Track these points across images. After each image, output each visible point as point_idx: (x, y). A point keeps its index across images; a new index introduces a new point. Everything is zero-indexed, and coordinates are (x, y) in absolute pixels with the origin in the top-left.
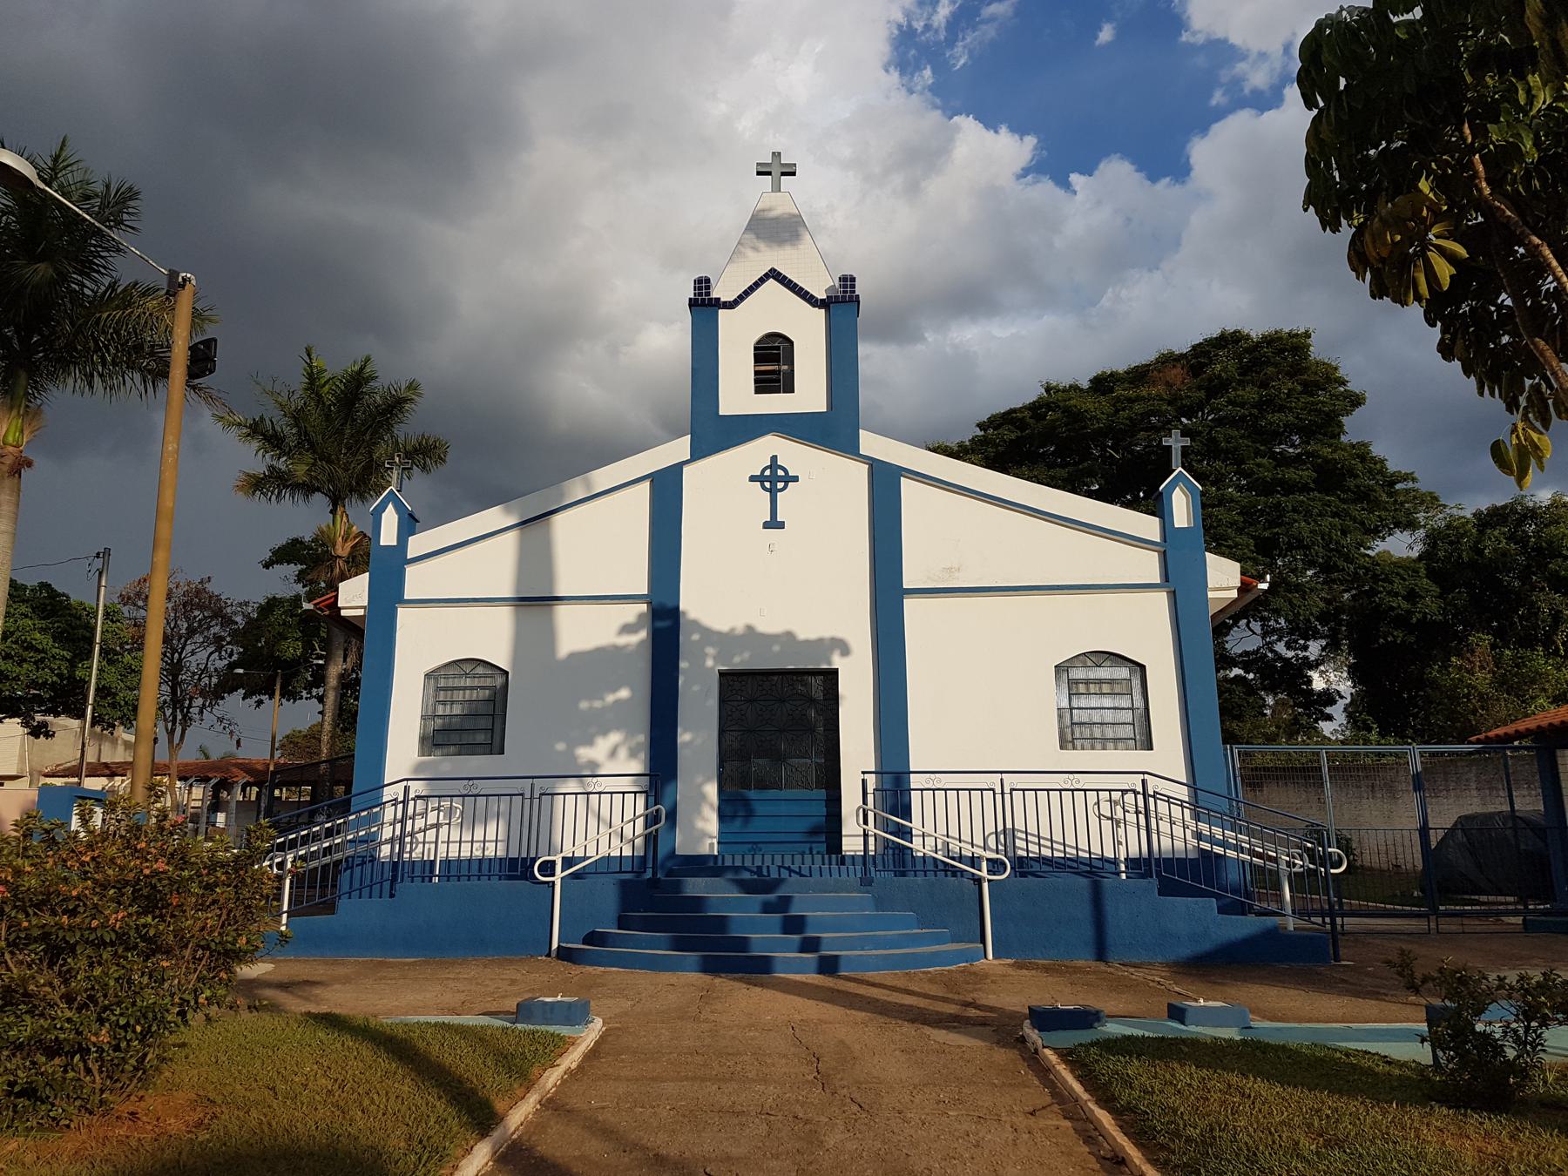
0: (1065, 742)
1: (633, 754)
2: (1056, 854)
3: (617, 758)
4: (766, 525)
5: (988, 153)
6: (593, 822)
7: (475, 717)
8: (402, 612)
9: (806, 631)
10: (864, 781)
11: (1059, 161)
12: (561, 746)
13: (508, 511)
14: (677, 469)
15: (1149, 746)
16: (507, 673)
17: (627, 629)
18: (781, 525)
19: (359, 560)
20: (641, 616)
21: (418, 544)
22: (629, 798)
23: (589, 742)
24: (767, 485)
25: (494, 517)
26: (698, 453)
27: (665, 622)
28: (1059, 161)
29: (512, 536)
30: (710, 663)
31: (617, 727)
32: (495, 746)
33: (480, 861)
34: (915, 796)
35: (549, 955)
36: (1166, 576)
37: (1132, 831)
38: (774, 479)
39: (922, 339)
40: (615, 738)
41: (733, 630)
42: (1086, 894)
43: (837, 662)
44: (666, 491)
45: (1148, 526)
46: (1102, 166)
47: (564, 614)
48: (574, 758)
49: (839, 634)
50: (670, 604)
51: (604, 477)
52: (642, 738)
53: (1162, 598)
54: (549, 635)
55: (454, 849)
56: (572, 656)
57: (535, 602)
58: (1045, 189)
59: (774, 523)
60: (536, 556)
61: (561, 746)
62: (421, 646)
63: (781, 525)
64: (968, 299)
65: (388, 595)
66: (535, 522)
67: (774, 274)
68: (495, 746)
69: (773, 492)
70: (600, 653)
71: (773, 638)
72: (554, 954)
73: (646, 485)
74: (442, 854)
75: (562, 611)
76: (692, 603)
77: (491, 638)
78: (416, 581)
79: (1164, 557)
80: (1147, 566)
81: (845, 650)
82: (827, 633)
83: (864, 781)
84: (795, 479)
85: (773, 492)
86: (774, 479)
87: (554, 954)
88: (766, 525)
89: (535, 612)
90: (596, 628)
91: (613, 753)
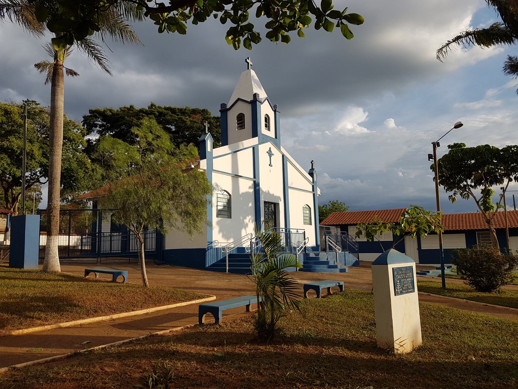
14: (257, 145)
18: (272, 166)
26: (260, 143)
36: (313, 190)
44: (255, 149)
52: (254, 218)
53: (312, 195)
73: (252, 148)
75: (240, 179)
79: (313, 186)
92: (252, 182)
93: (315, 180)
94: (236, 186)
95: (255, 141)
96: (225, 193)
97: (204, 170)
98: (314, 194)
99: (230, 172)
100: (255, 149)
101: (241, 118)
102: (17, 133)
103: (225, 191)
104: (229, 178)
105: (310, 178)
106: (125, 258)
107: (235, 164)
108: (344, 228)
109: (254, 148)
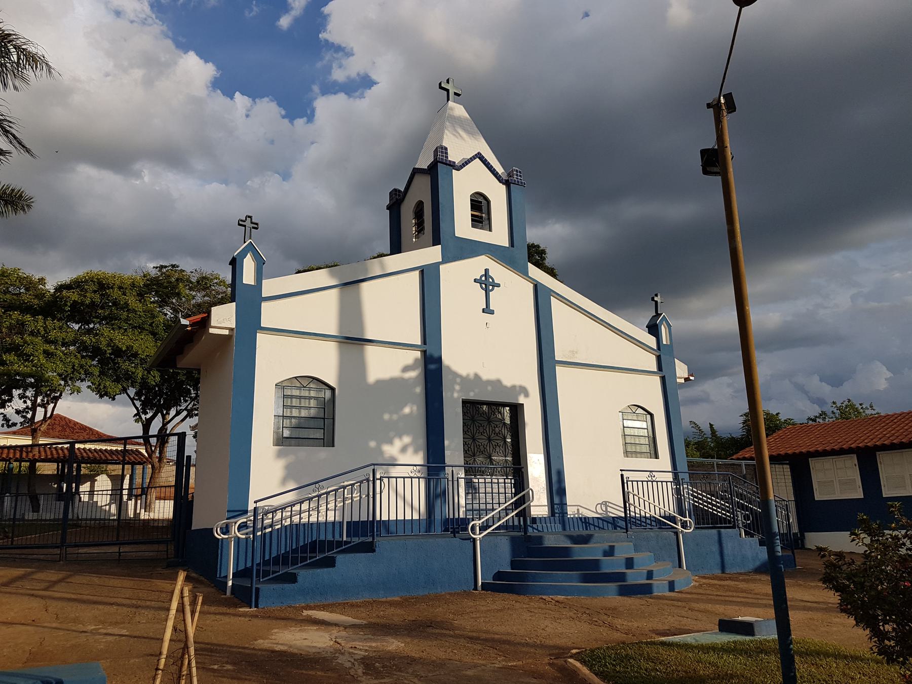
0: (627, 453)
1: (416, 451)
3: (405, 456)
5: (195, 70)
6: (408, 497)
7: (316, 421)
8: (260, 337)
9: (508, 382)
10: (622, 475)
11: (225, 85)
12: (373, 444)
13: (333, 275)
14: (435, 267)
15: (657, 457)
16: (333, 389)
17: (406, 369)
18: (492, 312)
19: (233, 292)
20: (416, 360)
21: (270, 287)
22: (415, 481)
23: (390, 442)
25: (321, 277)
26: (446, 259)
27: (432, 368)
28: (225, 85)
29: (334, 291)
30: (456, 395)
31: (407, 433)
32: (329, 441)
33: (334, 523)
35: (476, 588)
36: (660, 368)
38: (487, 283)
39: (138, 175)
40: (407, 440)
41: (468, 375)
42: (716, 538)
43: (521, 400)
44: (429, 279)
46: (266, 99)
48: (381, 453)
49: (524, 384)
50: (436, 355)
52: (422, 441)
53: (657, 380)
54: (361, 367)
55: (331, 515)
56: (379, 382)
57: (352, 341)
58: (219, 98)
59: (487, 310)
60: (351, 311)
61: (373, 444)
62: (276, 363)
63: (492, 312)
64: (171, 157)
65: (249, 323)
66: (350, 285)
67: (479, 156)
68: (329, 441)
70: (393, 381)
71: (489, 382)
72: (479, 588)
73: (417, 273)
74: (347, 519)
75: (370, 349)
77: (324, 362)
78: (270, 314)
79: (659, 358)
81: (525, 391)
82: (518, 383)
83: (622, 475)
84: (498, 285)
87: (479, 588)
88: (484, 311)
89: (353, 349)
90: (388, 365)
91: (404, 450)
92: (418, 354)
93: (665, 340)
94: (352, 367)
95: (433, 254)
96: (640, 411)
97: (231, 330)
98: (663, 379)
99: (333, 332)
100: (429, 279)
101: (419, 213)
102: (116, 319)
103: (639, 407)
104: (331, 349)
105: (651, 341)
106: (62, 510)
107: (351, 311)
108: (799, 466)
109: (422, 273)
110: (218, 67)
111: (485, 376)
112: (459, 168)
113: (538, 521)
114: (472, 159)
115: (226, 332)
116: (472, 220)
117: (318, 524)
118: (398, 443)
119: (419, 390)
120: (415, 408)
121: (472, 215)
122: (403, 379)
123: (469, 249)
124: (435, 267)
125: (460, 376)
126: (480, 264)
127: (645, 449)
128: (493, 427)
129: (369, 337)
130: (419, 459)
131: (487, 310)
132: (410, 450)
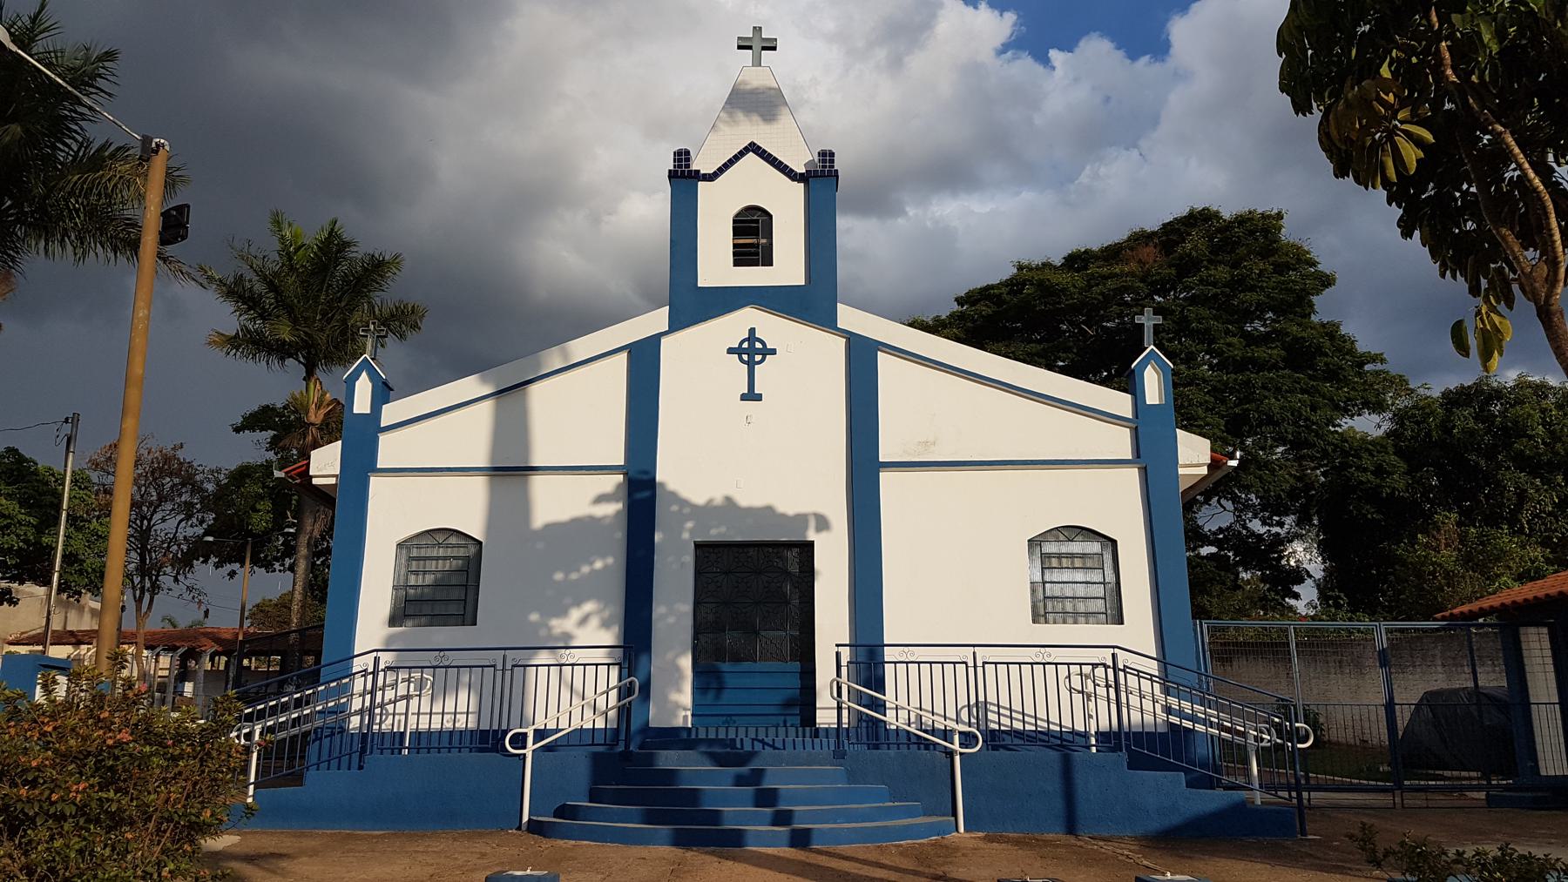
1: (605, 624)
2: (1028, 727)
4: (744, 398)
6: (565, 694)
7: (447, 587)
10: (838, 654)
12: (534, 617)
13: (484, 381)
14: (653, 343)
17: (601, 499)
18: (759, 398)
20: (619, 486)
21: (391, 412)
22: (603, 670)
23: (563, 612)
24: (745, 357)
25: (470, 386)
26: (676, 325)
29: (488, 405)
30: (686, 536)
32: (467, 616)
33: (440, 732)
34: (889, 669)
35: (519, 828)
37: (1103, 704)
38: (752, 351)
43: (811, 535)
44: (644, 363)
45: (1120, 403)
47: (539, 485)
51: (581, 347)
52: (617, 609)
53: (1133, 474)
54: (524, 506)
55: (424, 720)
56: (550, 528)
57: (510, 471)
58: (1025, 66)
62: (393, 516)
63: (759, 398)
64: (949, 173)
65: (361, 464)
66: (511, 393)
67: (753, 148)
68: (467, 616)
69: (751, 365)
72: (524, 828)
73: (624, 356)
74: (412, 725)
76: (669, 472)
77: (465, 508)
78: (389, 450)
80: (1119, 442)
81: (823, 524)
83: (838, 654)
84: (773, 352)
85: (751, 365)
86: (752, 351)
87: (524, 828)
88: (744, 398)
89: (510, 482)
90: (569, 500)
110: (1017, 9)
111: (744, 500)
112: (711, 178)
113: (821, 734)
114: (742, 154)
115: (333, 481)
116: (735, 254)
117: (429, 733)
118: (576, 614)
119: (620, 535)
120: (610, 560)
121: (735, 246)
122: (592, 520)
123: (726, 300)
124: (653, 343)
125: (694, 507)
126: (748, 318)
127: (1098, 606)
128: (754, 585)
129: (536, 462)
130: (609, 637)
131: (751, 396)
132: (594, 622)
